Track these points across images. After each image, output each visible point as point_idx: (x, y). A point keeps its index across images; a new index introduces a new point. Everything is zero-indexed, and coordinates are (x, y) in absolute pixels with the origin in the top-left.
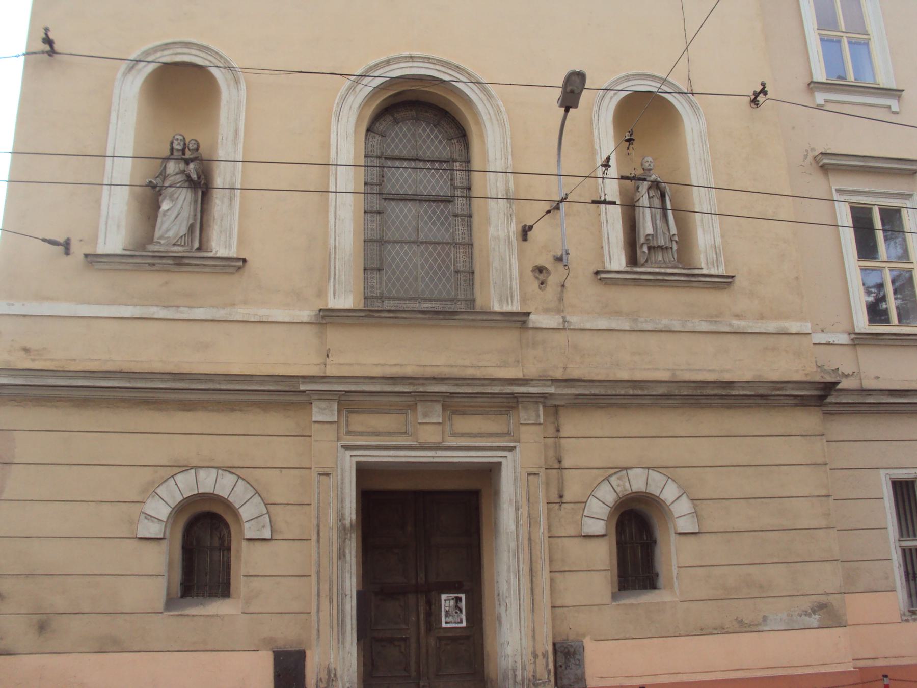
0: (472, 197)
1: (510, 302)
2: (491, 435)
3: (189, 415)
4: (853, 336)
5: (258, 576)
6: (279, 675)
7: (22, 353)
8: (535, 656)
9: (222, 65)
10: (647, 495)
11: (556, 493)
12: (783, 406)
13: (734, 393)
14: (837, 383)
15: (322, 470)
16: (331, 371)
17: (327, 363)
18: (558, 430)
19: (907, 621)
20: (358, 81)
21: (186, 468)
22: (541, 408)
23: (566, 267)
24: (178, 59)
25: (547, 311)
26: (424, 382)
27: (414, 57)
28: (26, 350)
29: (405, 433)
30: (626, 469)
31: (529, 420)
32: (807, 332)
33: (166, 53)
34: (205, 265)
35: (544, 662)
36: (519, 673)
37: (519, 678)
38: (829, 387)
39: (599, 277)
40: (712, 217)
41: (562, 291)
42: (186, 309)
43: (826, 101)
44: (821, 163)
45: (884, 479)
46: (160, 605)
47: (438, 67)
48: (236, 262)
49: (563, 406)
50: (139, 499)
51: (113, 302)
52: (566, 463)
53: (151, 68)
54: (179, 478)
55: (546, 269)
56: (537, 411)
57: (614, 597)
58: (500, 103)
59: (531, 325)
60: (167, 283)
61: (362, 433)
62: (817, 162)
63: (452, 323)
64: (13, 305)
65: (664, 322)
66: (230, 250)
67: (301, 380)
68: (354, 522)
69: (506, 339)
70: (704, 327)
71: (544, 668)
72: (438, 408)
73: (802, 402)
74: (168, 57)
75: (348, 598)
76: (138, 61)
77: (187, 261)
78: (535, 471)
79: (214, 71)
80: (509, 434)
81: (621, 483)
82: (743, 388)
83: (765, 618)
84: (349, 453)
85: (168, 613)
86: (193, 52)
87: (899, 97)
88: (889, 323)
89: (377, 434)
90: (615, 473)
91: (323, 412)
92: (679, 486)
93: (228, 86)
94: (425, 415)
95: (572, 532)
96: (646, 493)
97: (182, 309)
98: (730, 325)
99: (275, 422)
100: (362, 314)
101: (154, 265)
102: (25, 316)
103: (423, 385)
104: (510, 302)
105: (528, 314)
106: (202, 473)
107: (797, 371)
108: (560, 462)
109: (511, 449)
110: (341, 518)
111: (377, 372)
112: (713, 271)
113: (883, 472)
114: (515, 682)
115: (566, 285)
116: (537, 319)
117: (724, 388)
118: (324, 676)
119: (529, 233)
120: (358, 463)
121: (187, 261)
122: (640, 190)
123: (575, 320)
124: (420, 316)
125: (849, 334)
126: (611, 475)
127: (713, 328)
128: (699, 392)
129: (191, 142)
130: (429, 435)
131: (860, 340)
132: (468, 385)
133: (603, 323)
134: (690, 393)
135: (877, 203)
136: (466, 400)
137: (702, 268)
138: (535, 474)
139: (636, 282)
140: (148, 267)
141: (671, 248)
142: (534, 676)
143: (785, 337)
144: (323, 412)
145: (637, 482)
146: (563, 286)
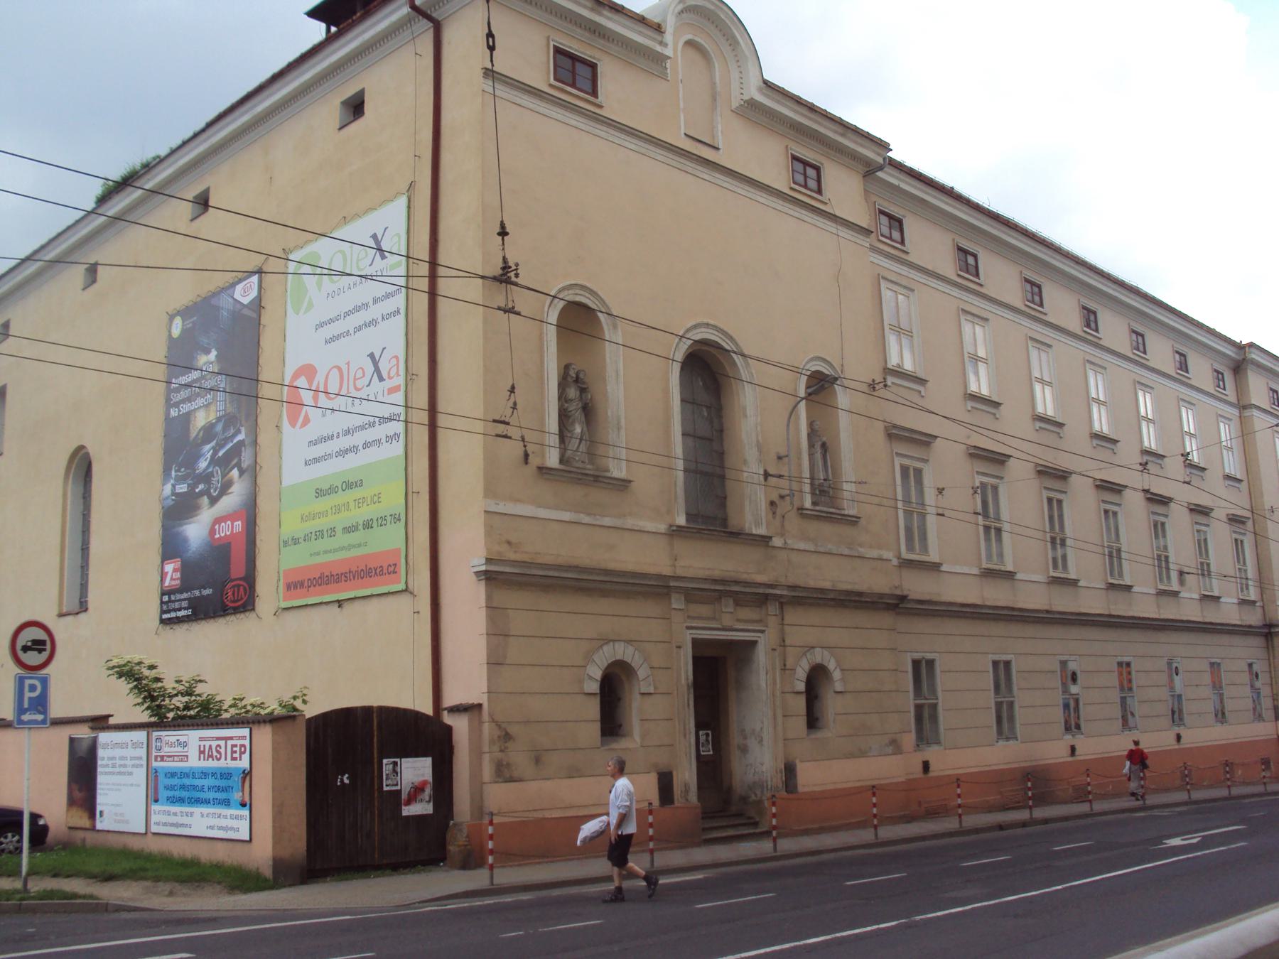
0: (265, 273)
9: (604, 311)
13: (863, 599)
16: (680, 572)
18: (783, 620)
28: (509, 543)
29: (714, 619)
33: (570, 292)
36: (769, 783)
37: (769, 787)
40: (345, 264)
44: (890, 432)
47: (720, 335)
50: (582, 664)
51: (557, 508)
52: (788, 642)
54: (605, 648)
58: (754, 372)
62: (887, 431)
64: (498, 504)
66: (621, 472)
70: (846, 552)
71: (778, 780)
72: (731, 602)
74: (570, 296)
89: (700, 618)
91: (677, 602)
93: (609, 330)
95: (790, 690)
99: (651, 608)
100: (695, 531)
106: (617, 645)
109: (763, 632)
111: (701, 574)
114: (768, 790)
115: (786, 516)
119: (29, 261)
120: (693, 639)
124: (723, 534)
128: (848, 598)
130: (727, 620)
132: (750, 587)
144: (677, 602)
145: (819, 656)
146: (783, 517)
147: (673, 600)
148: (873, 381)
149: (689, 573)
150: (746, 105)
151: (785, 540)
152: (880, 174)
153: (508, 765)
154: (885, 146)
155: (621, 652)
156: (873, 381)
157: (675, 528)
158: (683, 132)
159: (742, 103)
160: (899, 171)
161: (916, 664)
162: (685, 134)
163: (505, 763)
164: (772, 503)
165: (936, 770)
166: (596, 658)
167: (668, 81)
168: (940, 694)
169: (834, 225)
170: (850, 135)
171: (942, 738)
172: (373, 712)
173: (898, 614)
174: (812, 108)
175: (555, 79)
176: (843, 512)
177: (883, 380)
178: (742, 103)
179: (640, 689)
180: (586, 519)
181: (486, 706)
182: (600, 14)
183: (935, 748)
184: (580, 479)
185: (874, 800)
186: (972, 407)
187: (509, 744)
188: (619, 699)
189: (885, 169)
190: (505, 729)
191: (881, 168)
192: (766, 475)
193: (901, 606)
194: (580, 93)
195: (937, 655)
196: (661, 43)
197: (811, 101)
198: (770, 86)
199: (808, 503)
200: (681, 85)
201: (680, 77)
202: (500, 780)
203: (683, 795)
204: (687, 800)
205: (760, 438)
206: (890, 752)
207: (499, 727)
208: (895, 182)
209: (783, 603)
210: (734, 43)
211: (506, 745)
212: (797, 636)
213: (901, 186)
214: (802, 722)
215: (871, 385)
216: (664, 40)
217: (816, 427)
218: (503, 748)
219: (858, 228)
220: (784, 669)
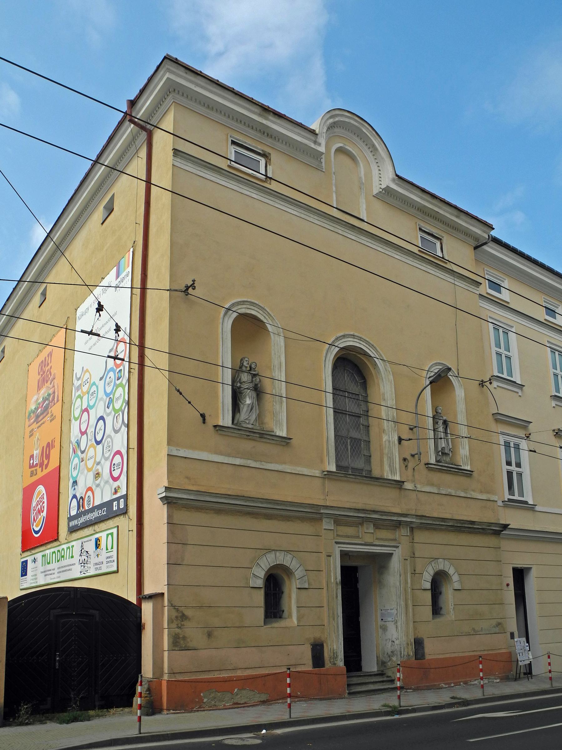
1: (395, 475)
6: (314, 656)
12: (429, 529)
14: (508, 525)
20: (429, 369)
21: (270, 550)
23: (419, 461)
24: (249, 311)
26: (370, 512)
27: (355, 336)
29: (358, 537)
32: (496, 500)
34: (273, 440)
35: (411, 647)
39: (427, 466)
42: (265, 463)
43: (498, 386)
52: (416, 555)
53: (235, 315)
54: (268, 555)
60: (254, 447)
63: (376, 483)
64: (179, 450)
67: (322, 507)
69: (393, 493)
70: (462, 494)
75: (339, 617)
77: (265, 436)
78: (406, 558)
79: (268, 326)
81: (435, 565)
82: (478, 525)
89: (348, 537)
91: (327, 524)
92: (455, 568)
94: (367, 529)
96: (444, 570)
97: (263, 463)
98: (471, 494)
99: (306, 528)
101: (249, 436)
102: (186, 458)
103: (369, 514)
105: (403, 482)
108: (414, 554)
109: (397, 547)
112: (466, 468)
116: (408, 486)
117: (472, 524)
121: (265, 436)
123: (419, 487)
129: (253, 364)
130: (368, 539)
132: (385, 515)
134: (460, 525)
136: (381, 522)
137: (461, 466)
139: (440, 470)
140: (245, 437)
141: (449, 454)
144: (327, 524)
145: (442, 565)
146: (414, 469)
151: (415, 485)
153: (184, 638)
157: (326, 473)
159: (381, 190)
163: (181, 636)
167: (324, 172)
170: (463, 216)
176: (460, 467)
178: (381, 190)
182: (267, 119)
186: (556, 405)
190: (182, 612)
196: (315, 142)
202: (176, 649)
207: (177, 610)
214: (428, 610)
218: (180, 625)
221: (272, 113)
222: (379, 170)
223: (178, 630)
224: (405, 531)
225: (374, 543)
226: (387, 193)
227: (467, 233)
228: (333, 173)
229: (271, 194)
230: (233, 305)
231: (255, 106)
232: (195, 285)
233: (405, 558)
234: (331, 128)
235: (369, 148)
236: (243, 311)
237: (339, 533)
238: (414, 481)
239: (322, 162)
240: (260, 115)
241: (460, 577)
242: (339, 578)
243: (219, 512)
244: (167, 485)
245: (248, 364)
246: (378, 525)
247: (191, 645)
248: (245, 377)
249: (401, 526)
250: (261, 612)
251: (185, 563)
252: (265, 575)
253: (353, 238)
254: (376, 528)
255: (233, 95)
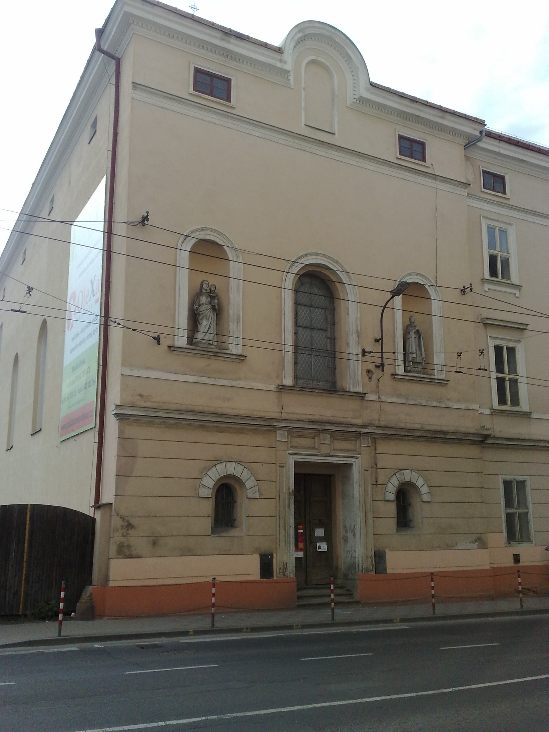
1: (357, 386)
2: (351, 450)
3: (222, 435)
4: (492, 411)
5: (253, 516)
7: (139, 397)
8: (367, 558)
10: (411, 483)
11: (375, 480)
15: (280, 465)
16: (284, 416)
17: (282, 412)
18: (375, 450)
19: (507, 546)
21: (221, 462)
22: (370, 438)
24: (208, 237)
25: (372, 392)
29: (314, 448)
30: (402, 470)
31: (365, 444)
33: (202, 233)
38: (487, 436)
39: (393, 377)
41: (378, 382)
43: (489, 289)
45: (500, 479)
46: (209, 532)
48: (243, 357)
49: (378, 438)
52: (379, 466)
53: (193, 241)
54: (218, 466)
55: (372, 371)
56: (368, 440)
57: (397, 531)
59: (365, 399)
60: (208, 365)
61: (296, 447)
63: (334, 395)
65: (419, 401)
67: (274, 420)
68: (293, 491)
69: (354, 404)
70: (435, 404)
71: (369, 563)
72: (329, 436)
73: (473, 443)
74: (201, 236)
76: (188, 236)
77: (219, 355)
78: (367, 469)
79: (226, 248)
80: (356, 450)
81: (400, 476)
83: (456, 544)
84: (291, 456)
85: (213, 535)
86: (215, 234)
87: (520, 289)
88: (519, 406)
89: (303, 448)
90: (398, 472)
91: (281, 436)
94: (324, 440)
101: (203, 355)
104: (357, 386)
106: (228, 464)
107: (472, 428)
108: (376, 465)
109: (357, 458)
110: (289, 489)
111: (304, 417)
113: (500, 477)
116: (372, 397)
118: (282, 567)
121: (219, 355)
122: (410, 333)
123: (383, 398)
125: (490, 409)
126: (397, 472)
127: (438, 405)
130: (325, 449)
131: (495, 413)
133: (394, 400)
135: (505, 344)
138: (367, 470)
140: (199, 356)
142: (367, 567)
143: (468, 411)
144: (281, 436)
145: (407, 476)
146: (379, 380)
147: (278, 435)
148: (464, 287)
149: (291, 417)
150: (358, 102)
151: (379, 396)
152: (480, 144)
153: (129, 546)
154: (482, 123)
155: (232, 469)
156: (464, 287)
157: (281, 387)
158: (303, 122)
159: (355, 100)
160: (498, 141)
161: (507, 484)
162: (305, 125)
163: (126, 544)
164: (369, 371)
165: (525, 561)
166: (210, 473)
167: (293, 89)
168: (530, 505)
169: (434, 182)
170: (448, 116)
171: (533, 537)
172: (27, 508)
173: (483, 447)
174: (414, 100)
175: (400, 154)
176: (433, 377)
177: (470, 286)
179: (247, 495)
180: (207, 381)
181: (113, 504)
182: (229, 42)
183: (525, 545)
184: (203, 355)
185: (520, 580)
187: (131, 532)
188: (235, 502)
189: (483, 140)
190: (128, 521)
191: (479, 140)
192: (364, 352)
193: (485, 442)
194: (215, 99)
195: (528, 477)
196: (281, 61)
197: (388, 86)
198: (375, 86)
199: (401, 370)
200: (303, 92)
201: (303, 86)
202: (120, 556)
203: (281, 571)
204: (284, 575)
205: (359, 328)
206: (476, 547)
207: (123, 519)
208: (496, 150)
209: (374, 439)
210: (348, 59)
211: (128, 532)
212: (384, 461)
213: (501, 152)
214: (391, 524)
215: (463, 290)
216: (282, 58)
217: (413, 321)
218: (125, 534)
219: (456, 182)
220: (376, 483)
221: (233, 37)
222: (354, 79)
223: (124, 539)
224: (365, 442)
225: (331, 454)
226: (361, 103)
227: (455, 132)
228: (303, 89)
229: (250, 123)
230: (192, 232)
231: (216, 31)
232: (148, 217)
233: (365, 468)
234: (301, 42)
235: (344, 57)
236: (202, 237)
237: (294, 444)
238: (378, 393)
239: (289, 80)
240: (222, 39)
241: (430, 489)
242: (292, 487)
243: (170, 426)
244: (118, 403)
245: (208, 288)
246: (336, 435)
247: (134, 553)
248: (204, 299)
249: (362, 437)
250: (207, 523)
251: (134, 474)
252: (215, 485)
253: (322, 154)
254: (334, 439)
255: (193, 22)
